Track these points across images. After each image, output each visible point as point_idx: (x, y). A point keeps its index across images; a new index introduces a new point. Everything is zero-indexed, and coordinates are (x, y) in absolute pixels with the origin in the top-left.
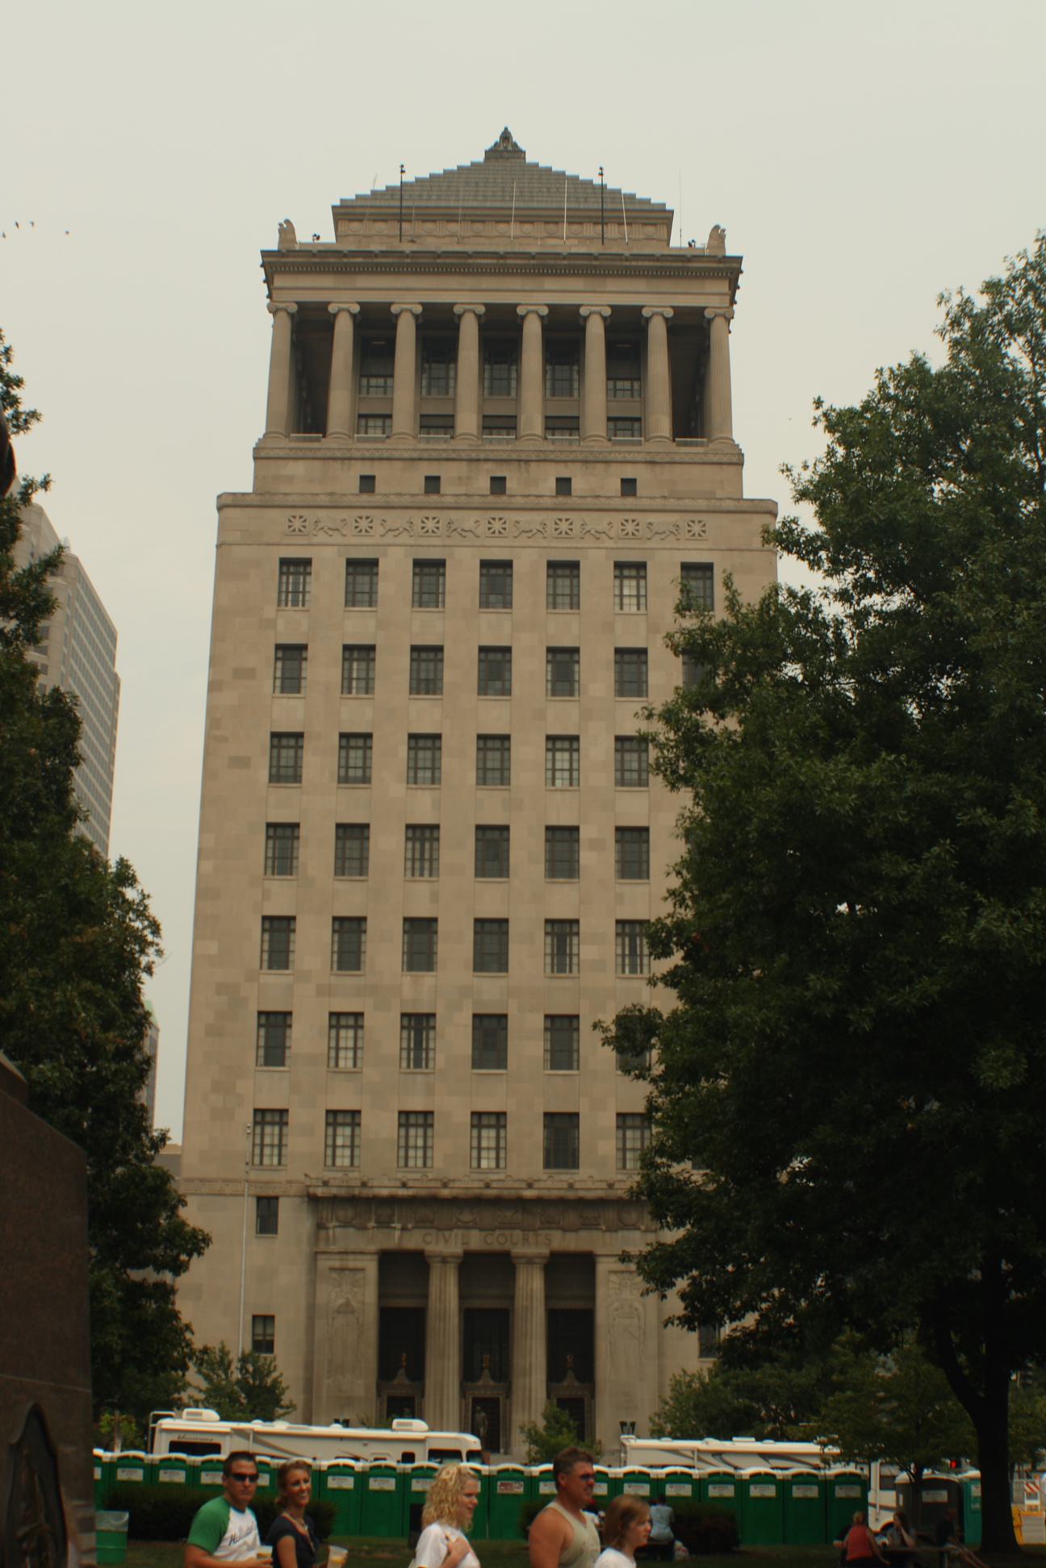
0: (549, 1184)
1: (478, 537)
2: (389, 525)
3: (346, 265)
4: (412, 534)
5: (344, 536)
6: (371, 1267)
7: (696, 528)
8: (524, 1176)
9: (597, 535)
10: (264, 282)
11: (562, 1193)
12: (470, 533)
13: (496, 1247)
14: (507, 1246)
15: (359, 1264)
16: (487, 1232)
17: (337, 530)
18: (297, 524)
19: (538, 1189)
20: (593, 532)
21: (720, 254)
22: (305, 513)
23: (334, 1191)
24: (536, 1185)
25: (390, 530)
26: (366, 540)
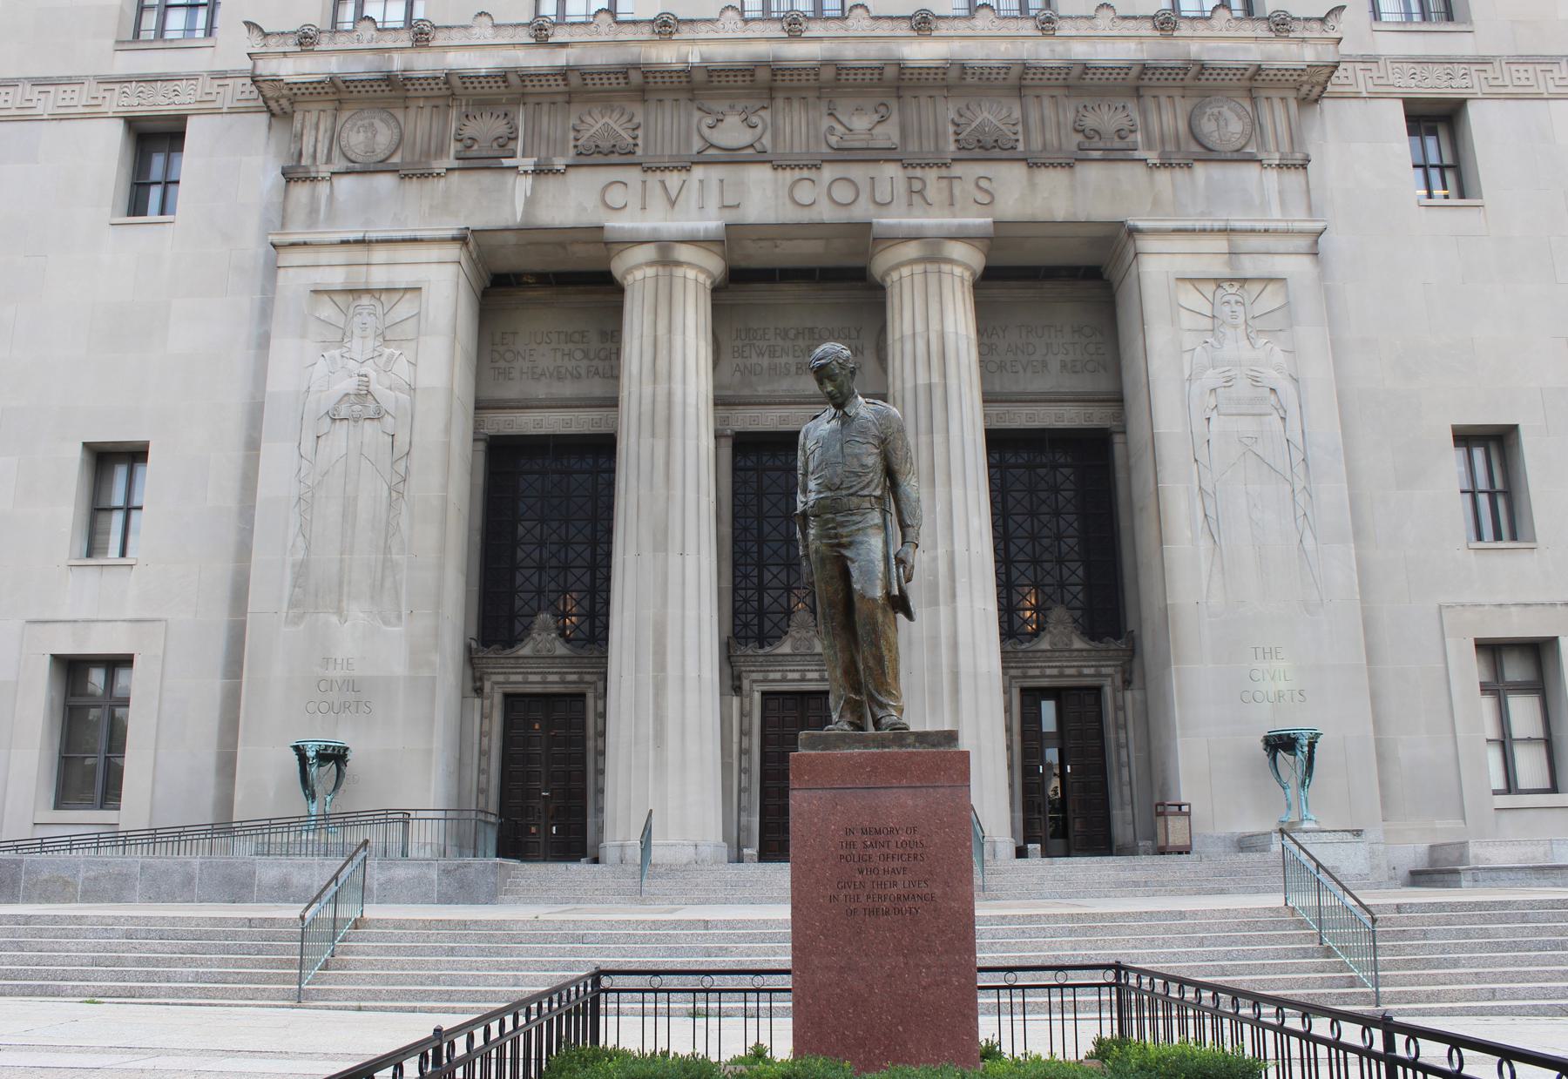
16: (797, 174)
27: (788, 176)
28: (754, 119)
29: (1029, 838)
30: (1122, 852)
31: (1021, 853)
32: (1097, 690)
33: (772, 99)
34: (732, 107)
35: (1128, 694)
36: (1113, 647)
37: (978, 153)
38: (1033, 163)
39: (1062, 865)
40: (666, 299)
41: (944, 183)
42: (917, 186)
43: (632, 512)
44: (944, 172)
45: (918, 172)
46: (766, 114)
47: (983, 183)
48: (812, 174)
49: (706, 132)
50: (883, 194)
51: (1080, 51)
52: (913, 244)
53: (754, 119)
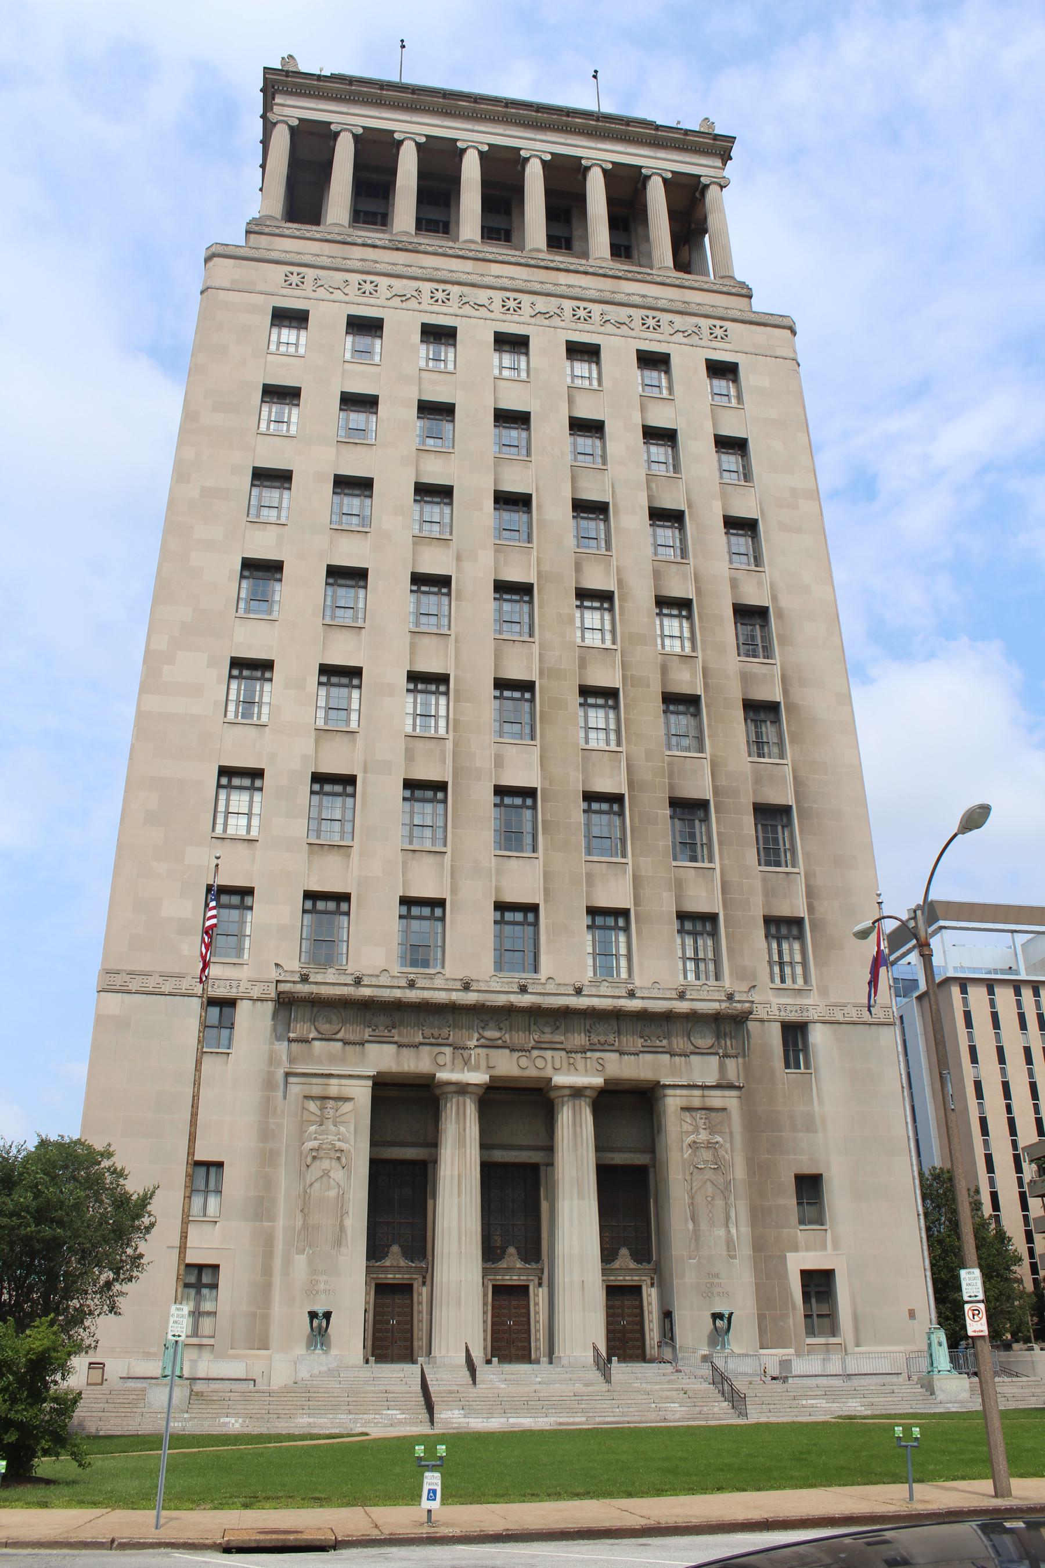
0: (495, 986)
1: (492, 312)
2: (676, 326)
3: (352, 92)
4: (563, 318)
5: (347, 295)
6: (362, 1093)
7: (651, 322)
8: (569, 980)
9: (331, 290)
10: (261, 91)
11: (398, 994)
12: (483, 308)
13: (532, 1072)
14: (548, 1072)
15: (348, 1092)
16: (521, 1054)
17: (625, 323)
18: (294, 279)
19: (478, 991)
20: (471, 303)
21: (710, 131)
22: (448, 287)
23: (366, 992)
24: (474, 986)
25: (396, 295)
26: (444, 309)
27: (516, 1055)
28: (502, 1026)
29: (493, 1356)
30: (651, 1361)
31: (489, 1362)
32: (527, 1287)
33: (510, 1015)
34: (492, 1018)
35: (540, 1289)
36: (535, 1267)
37: (598, 1047)
38: (622, 1053)
39: (508, 1368)
40: (461, 1116)
41: (583, 1060)
42: (572, 1061)
43: (566, 1224)
44: (583, 1055)
45: (573, 1055)
46: (507, 1023)
47: (601, 1061)
48: (528, 1054)
49: (481, 1031)
50: (441, 1060)
51: (427, 995)
52: (452, 1086)
53: (502, 1026)
